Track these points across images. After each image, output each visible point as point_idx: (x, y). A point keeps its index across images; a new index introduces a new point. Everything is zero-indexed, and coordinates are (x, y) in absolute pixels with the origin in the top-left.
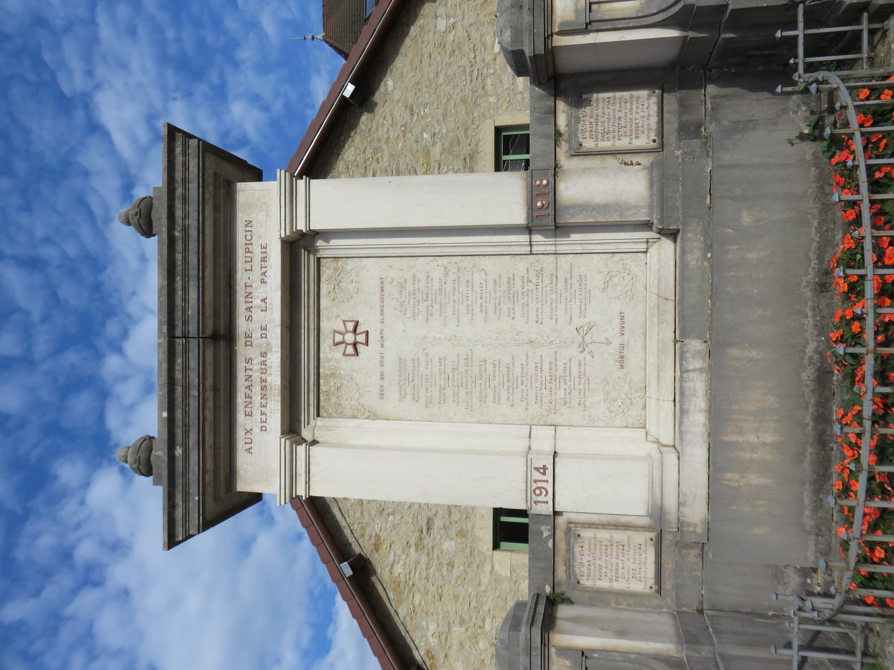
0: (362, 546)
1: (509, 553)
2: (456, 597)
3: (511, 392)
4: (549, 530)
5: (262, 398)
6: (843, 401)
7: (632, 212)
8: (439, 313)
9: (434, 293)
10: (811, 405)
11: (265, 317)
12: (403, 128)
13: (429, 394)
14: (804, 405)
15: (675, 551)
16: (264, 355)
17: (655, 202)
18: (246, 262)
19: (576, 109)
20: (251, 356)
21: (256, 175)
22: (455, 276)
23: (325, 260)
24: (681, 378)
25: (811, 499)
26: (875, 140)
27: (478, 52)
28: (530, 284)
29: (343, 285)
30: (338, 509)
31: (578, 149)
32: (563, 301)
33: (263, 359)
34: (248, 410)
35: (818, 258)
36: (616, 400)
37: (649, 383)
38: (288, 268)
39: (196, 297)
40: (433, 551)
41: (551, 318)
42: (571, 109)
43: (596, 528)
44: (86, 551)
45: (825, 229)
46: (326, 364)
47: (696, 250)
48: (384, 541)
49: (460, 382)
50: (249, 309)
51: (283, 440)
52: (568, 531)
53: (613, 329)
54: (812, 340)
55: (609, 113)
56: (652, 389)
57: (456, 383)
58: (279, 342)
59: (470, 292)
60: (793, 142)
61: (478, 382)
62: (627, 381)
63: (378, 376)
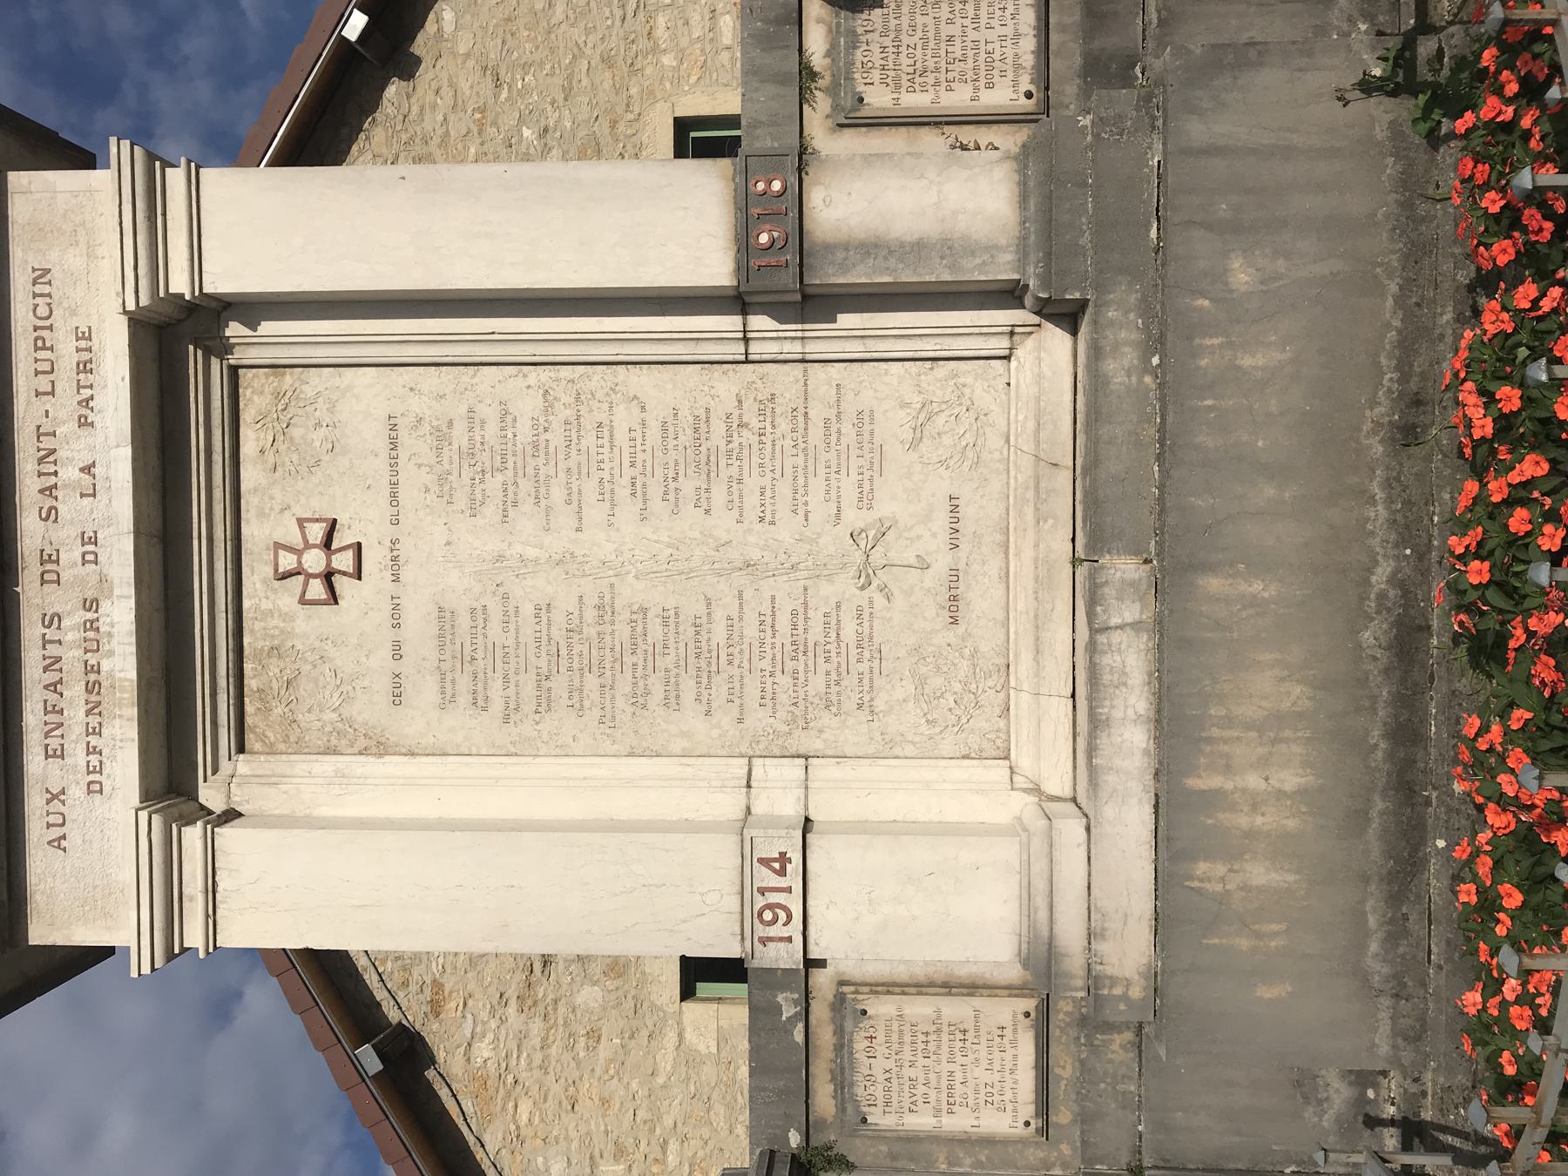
2: (605, 1102)
3: (705, 681)
4: (796, 1003)
5: (88, 713)
6: (1453, 692)
8: (532, 500)
10: (1382, 705)
11: (92, 512)
12: (478, 116)
13: (512, 690)
15: (1078, 1038)
16: (91, 604)
17: (1033, 237)
18: (37, 373)
20: (57, 609)
22: (568, 412)
23: (251, 373)
24: (1092, 647)
25: (1384, 916)
28: (745, 433)
29: (296, 432)
32: (821, 471)
33: (90, 615)
34: (54, 743)
35: (1397, 368)
37: (1016, 656)
40: (555, 1010)
41: (794, 511)
43: (903, 993)
45: (1414, 300)
46: (258, 626)
47: (1127, 349)
48: (451, 993)
49: (586, 662)
50: (48, 491)
51: (144, 815)
52: (839, 1002)
53: (934, 535)
54: (1385, 556)
55: (925, 25)
57: (576, 665)
58: (129, 572)
59: (606, 450)
60: (1348, 96)
61: (628, 660)
62: (967, 651)
63: (386, 652)
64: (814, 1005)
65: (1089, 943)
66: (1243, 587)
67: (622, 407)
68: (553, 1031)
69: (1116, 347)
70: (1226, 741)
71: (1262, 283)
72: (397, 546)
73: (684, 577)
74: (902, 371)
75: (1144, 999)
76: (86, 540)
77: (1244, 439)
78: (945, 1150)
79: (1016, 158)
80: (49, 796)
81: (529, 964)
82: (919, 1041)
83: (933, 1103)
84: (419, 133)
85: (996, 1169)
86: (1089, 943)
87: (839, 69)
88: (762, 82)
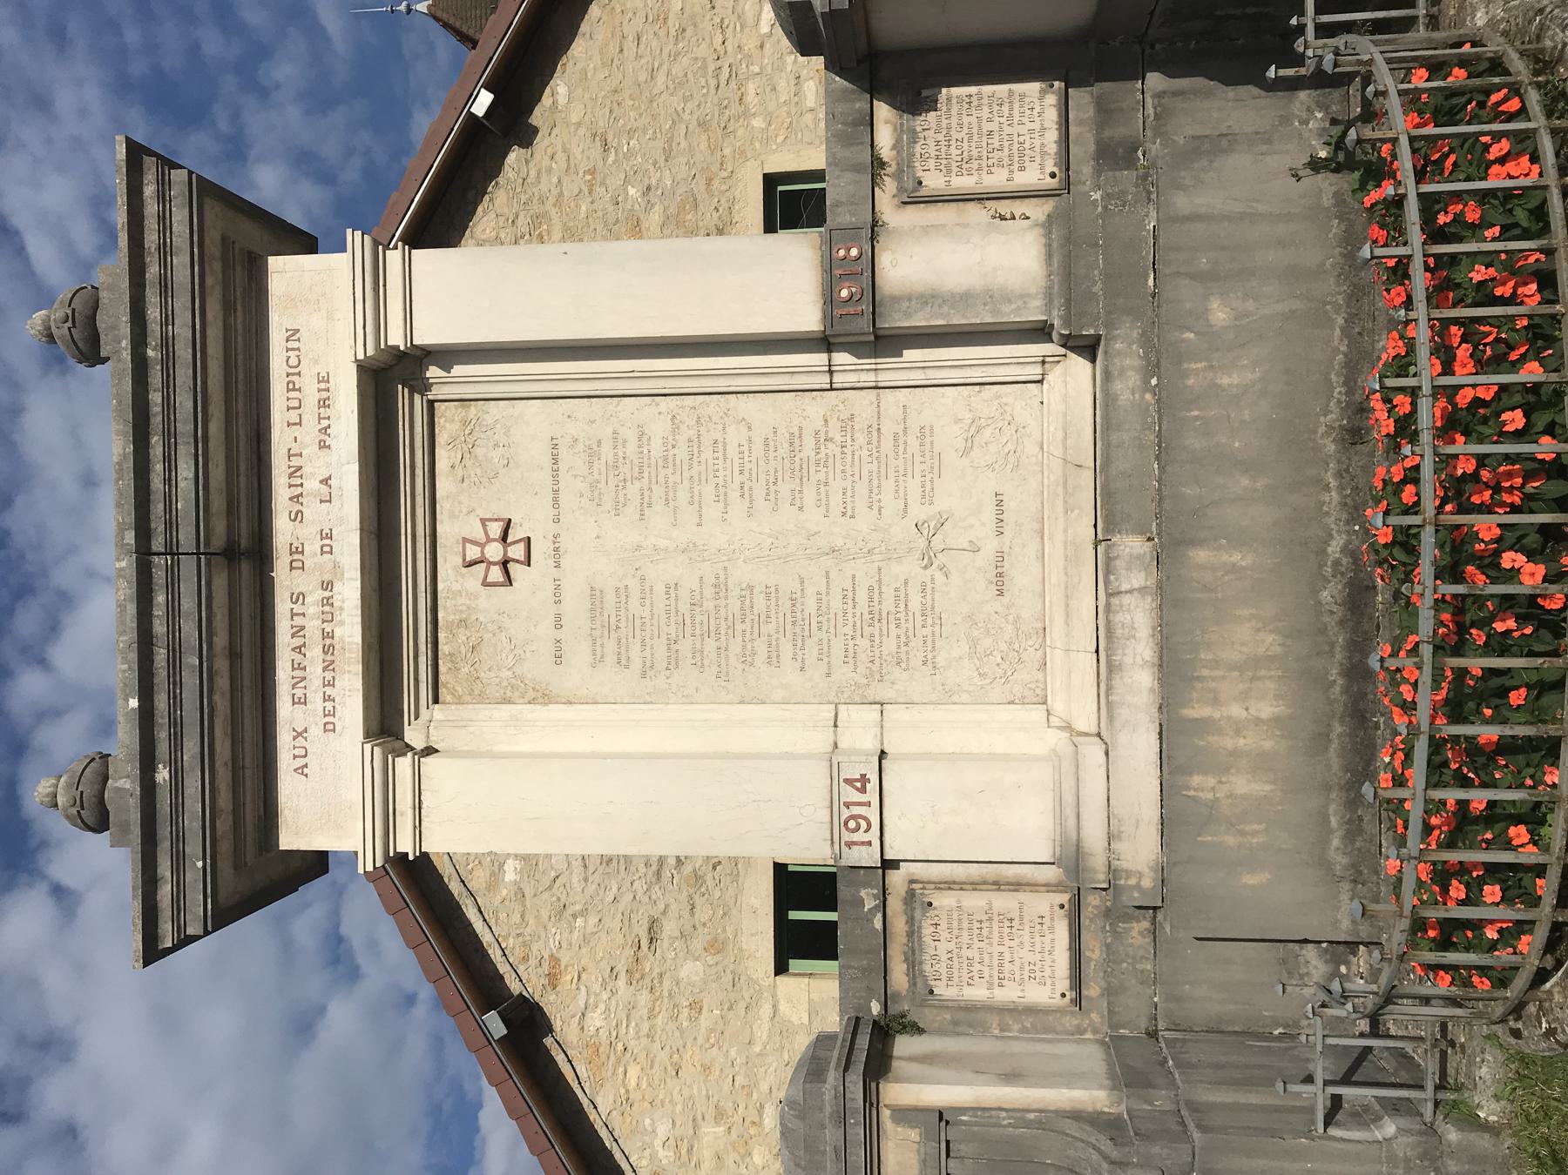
0: (523, 979)
1: (806, 980)
2: (706, 1069)
3: (799, 643)
4: (875, 897)
5: (325, 669)
7: (1014, 306)
9: (653, 465)
10: (1339, 649)
12: (588, 177)
13: (648, 653)
14: (1327, 648)
15: (1105, 927)
16: (327, 585)
17: (1056, 287)
18: (289, 409)
19: (910, 116)
21: (306, 244)
22: (691, 432)
24: (1108, 606)
25: (1343, 817)
26: (1436, 156)
27: (729, 32)
28: (830, 445)
29: (479, 451)
30: (476, 910)
31: (915, 190)
32: (891, 474)
33: (327, 594)
34: (299, 693)
35: (1345, 384)
36: (991, 654)
37: (1051, 621)
39: (191, 475)
42: (901, 117)
43: (961, 889)
45: (1357, 330)
47: (1130, 373)
49: (706, 629)
50: (296, 498)
51: (368, 747)
52: (910, 896)
53: (983, 524)
57: (698, 632)
59: (720, 461)
60: (1301, 173)
63: (549, 622)
64: (890, 899)
65: (1109, 844)
66: (1225, 558)
67: (734, 426)
68: (658, 1003)
69: (1122, 371)
70: (1214, 679)
71: (1236, 319)
72: (558, 540)
73: (782, 560)
74: (956, 394)
75: (1154, 887)
76: (324, 535)
77: (1224, 441)
78: (997, 1018)
79: (1042, 225)
80: (295, 734)
81: (637, 940)
82: (975, 928)
83: (987, 978)
84: (536, 194)
85: (1037, 1033)
86: (1109, 844)
87: (902, 160)
88: (842, 171)
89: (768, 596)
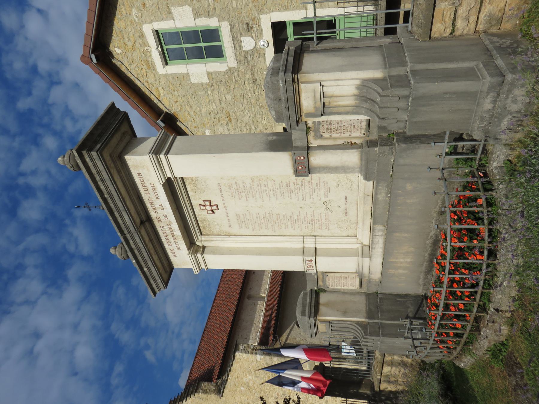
7: (350, 170)
28: (298, 185)
32: (316, 192)
38: (169, 192)
39: (128, 218)
44: (43, 66)
51: (190, 255)
56: (360, 225)
57: (266, 222)
61: (277, 222)
89: (284, 216)
